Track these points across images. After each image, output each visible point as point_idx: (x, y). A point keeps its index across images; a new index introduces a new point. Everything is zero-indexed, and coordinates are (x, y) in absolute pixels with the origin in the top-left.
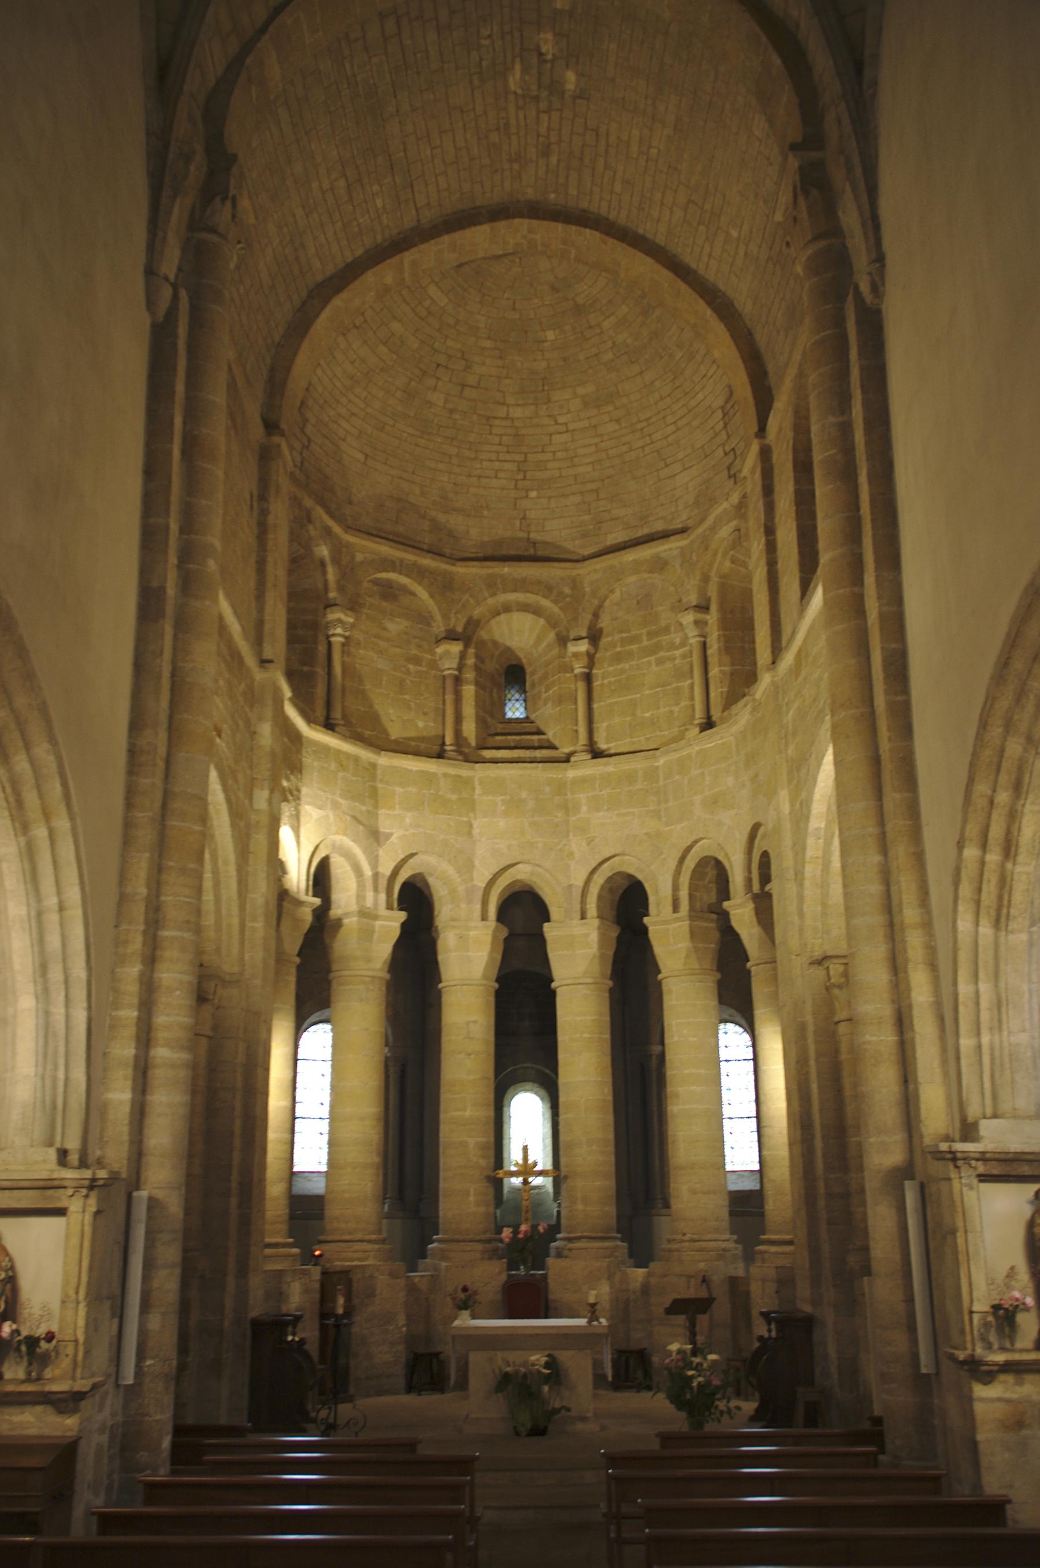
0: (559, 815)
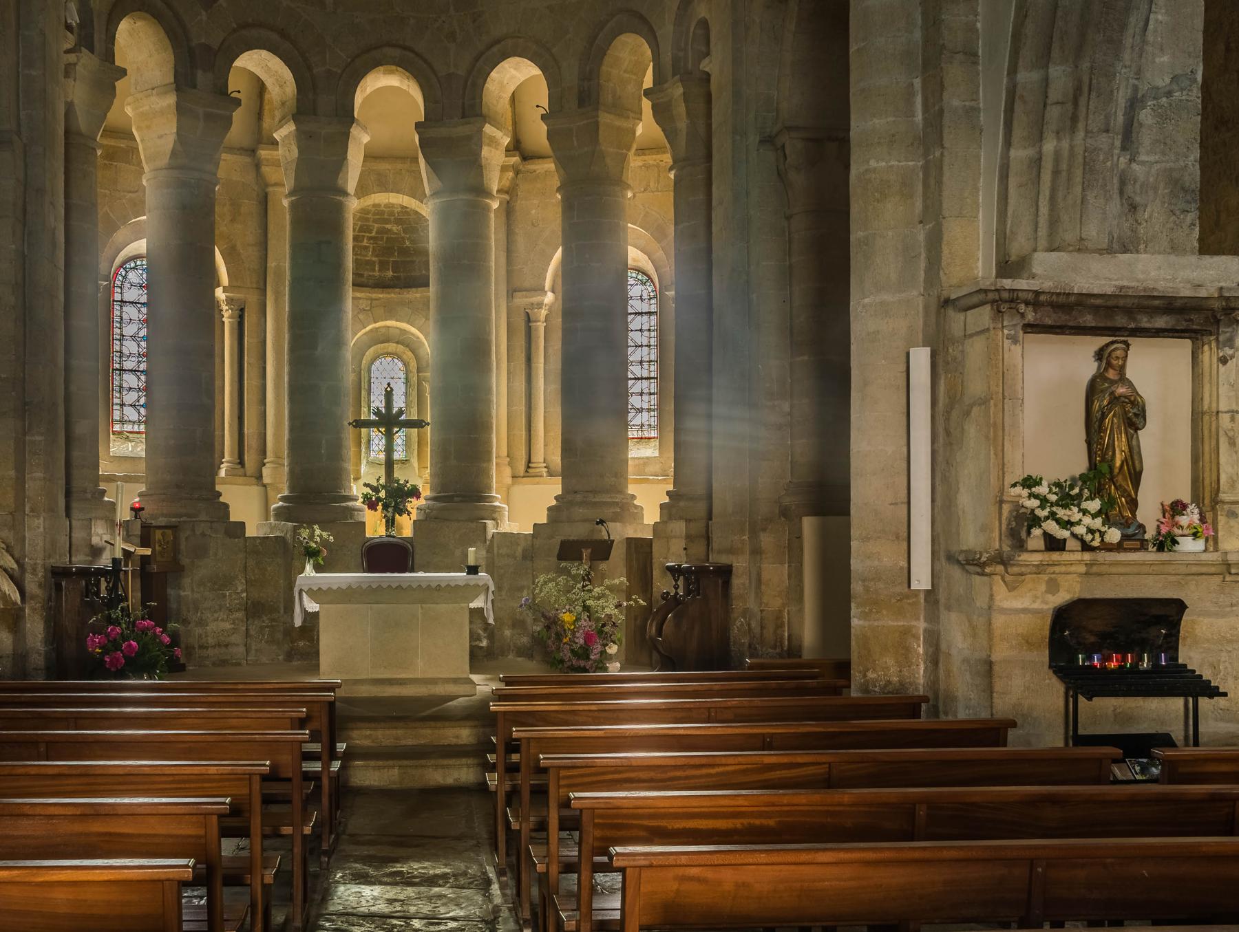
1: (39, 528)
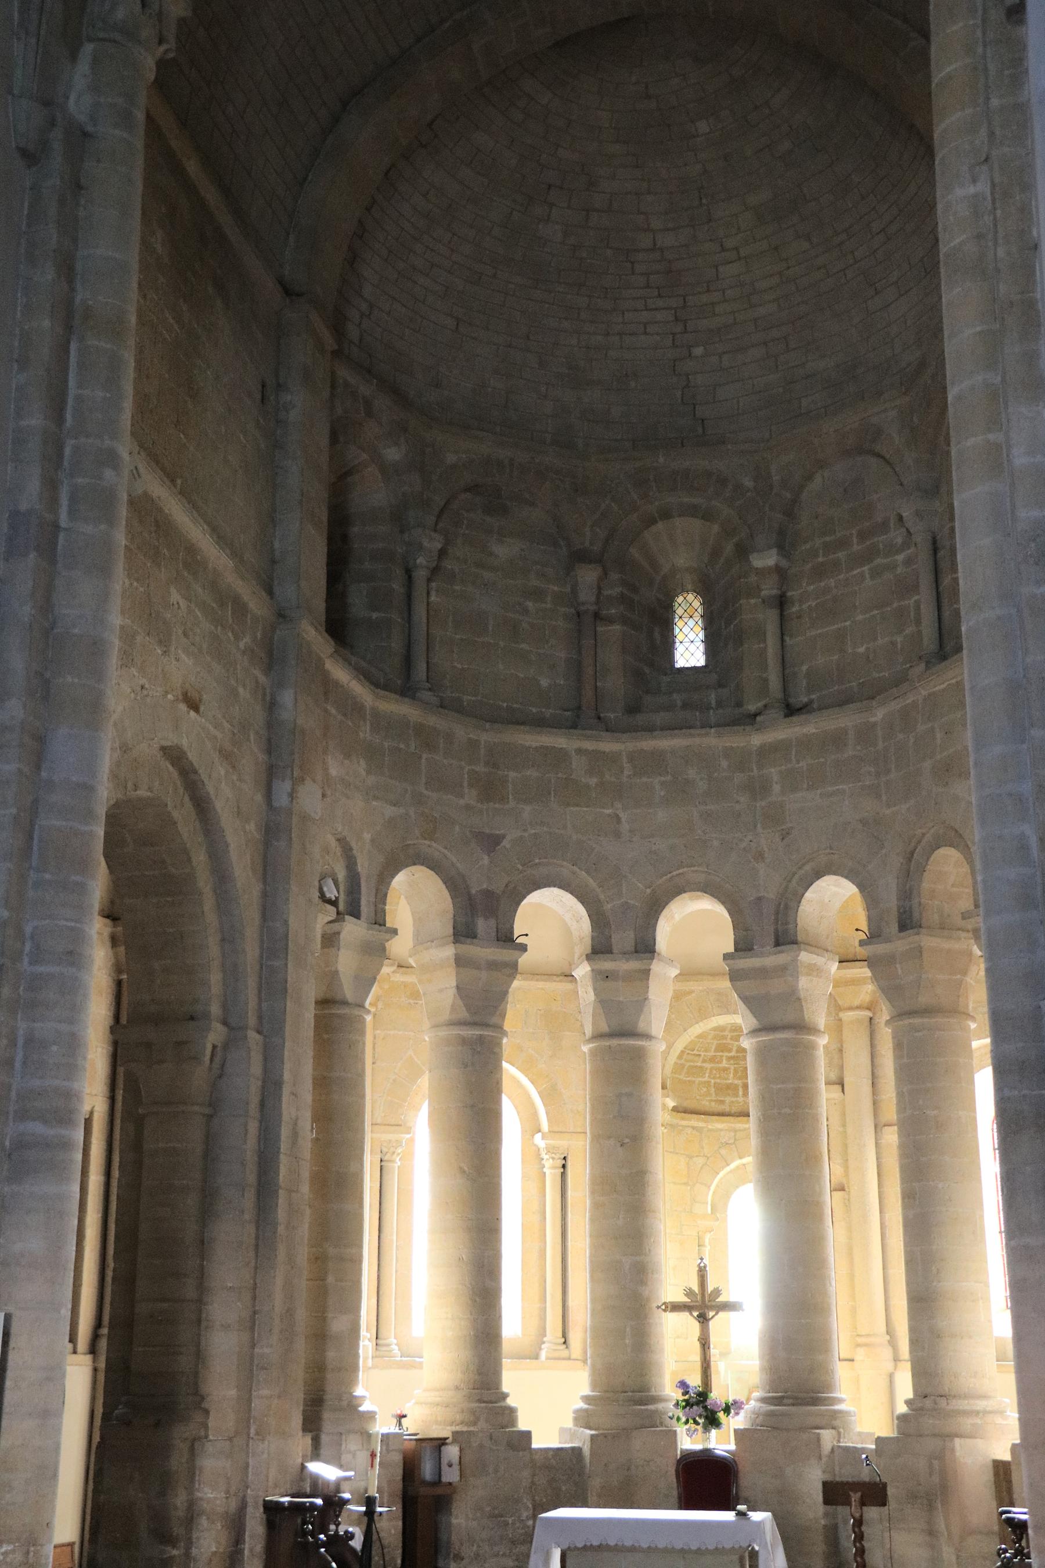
0: (742, 799)
1: (263, 1453)
